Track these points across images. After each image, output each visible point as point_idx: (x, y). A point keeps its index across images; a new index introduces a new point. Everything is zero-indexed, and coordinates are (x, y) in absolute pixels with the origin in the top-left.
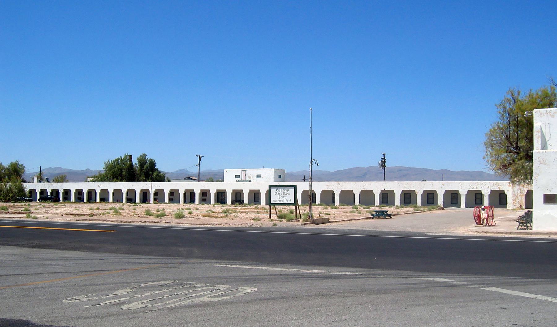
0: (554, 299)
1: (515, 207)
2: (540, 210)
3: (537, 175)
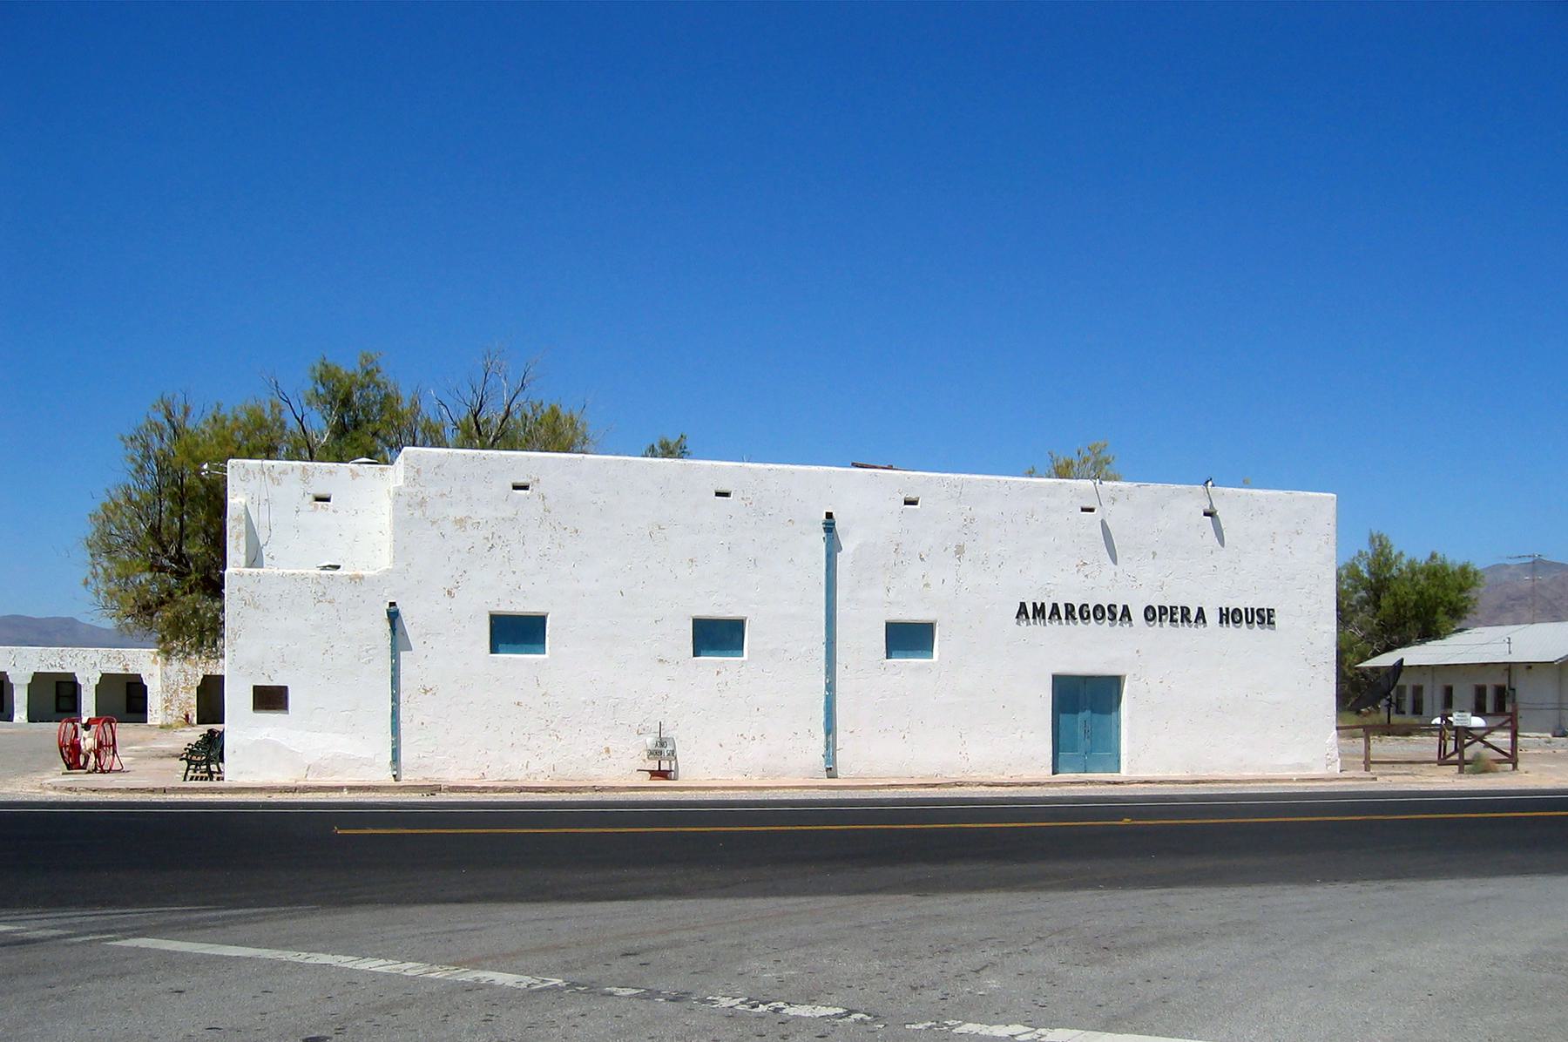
0: (304, 955)
1: (170, 720)
2: (242, 725)
3: (236, 635)
